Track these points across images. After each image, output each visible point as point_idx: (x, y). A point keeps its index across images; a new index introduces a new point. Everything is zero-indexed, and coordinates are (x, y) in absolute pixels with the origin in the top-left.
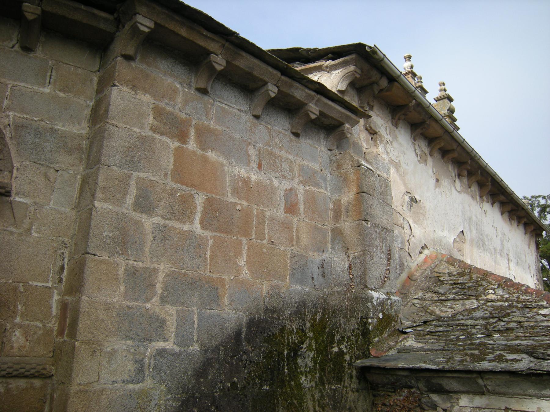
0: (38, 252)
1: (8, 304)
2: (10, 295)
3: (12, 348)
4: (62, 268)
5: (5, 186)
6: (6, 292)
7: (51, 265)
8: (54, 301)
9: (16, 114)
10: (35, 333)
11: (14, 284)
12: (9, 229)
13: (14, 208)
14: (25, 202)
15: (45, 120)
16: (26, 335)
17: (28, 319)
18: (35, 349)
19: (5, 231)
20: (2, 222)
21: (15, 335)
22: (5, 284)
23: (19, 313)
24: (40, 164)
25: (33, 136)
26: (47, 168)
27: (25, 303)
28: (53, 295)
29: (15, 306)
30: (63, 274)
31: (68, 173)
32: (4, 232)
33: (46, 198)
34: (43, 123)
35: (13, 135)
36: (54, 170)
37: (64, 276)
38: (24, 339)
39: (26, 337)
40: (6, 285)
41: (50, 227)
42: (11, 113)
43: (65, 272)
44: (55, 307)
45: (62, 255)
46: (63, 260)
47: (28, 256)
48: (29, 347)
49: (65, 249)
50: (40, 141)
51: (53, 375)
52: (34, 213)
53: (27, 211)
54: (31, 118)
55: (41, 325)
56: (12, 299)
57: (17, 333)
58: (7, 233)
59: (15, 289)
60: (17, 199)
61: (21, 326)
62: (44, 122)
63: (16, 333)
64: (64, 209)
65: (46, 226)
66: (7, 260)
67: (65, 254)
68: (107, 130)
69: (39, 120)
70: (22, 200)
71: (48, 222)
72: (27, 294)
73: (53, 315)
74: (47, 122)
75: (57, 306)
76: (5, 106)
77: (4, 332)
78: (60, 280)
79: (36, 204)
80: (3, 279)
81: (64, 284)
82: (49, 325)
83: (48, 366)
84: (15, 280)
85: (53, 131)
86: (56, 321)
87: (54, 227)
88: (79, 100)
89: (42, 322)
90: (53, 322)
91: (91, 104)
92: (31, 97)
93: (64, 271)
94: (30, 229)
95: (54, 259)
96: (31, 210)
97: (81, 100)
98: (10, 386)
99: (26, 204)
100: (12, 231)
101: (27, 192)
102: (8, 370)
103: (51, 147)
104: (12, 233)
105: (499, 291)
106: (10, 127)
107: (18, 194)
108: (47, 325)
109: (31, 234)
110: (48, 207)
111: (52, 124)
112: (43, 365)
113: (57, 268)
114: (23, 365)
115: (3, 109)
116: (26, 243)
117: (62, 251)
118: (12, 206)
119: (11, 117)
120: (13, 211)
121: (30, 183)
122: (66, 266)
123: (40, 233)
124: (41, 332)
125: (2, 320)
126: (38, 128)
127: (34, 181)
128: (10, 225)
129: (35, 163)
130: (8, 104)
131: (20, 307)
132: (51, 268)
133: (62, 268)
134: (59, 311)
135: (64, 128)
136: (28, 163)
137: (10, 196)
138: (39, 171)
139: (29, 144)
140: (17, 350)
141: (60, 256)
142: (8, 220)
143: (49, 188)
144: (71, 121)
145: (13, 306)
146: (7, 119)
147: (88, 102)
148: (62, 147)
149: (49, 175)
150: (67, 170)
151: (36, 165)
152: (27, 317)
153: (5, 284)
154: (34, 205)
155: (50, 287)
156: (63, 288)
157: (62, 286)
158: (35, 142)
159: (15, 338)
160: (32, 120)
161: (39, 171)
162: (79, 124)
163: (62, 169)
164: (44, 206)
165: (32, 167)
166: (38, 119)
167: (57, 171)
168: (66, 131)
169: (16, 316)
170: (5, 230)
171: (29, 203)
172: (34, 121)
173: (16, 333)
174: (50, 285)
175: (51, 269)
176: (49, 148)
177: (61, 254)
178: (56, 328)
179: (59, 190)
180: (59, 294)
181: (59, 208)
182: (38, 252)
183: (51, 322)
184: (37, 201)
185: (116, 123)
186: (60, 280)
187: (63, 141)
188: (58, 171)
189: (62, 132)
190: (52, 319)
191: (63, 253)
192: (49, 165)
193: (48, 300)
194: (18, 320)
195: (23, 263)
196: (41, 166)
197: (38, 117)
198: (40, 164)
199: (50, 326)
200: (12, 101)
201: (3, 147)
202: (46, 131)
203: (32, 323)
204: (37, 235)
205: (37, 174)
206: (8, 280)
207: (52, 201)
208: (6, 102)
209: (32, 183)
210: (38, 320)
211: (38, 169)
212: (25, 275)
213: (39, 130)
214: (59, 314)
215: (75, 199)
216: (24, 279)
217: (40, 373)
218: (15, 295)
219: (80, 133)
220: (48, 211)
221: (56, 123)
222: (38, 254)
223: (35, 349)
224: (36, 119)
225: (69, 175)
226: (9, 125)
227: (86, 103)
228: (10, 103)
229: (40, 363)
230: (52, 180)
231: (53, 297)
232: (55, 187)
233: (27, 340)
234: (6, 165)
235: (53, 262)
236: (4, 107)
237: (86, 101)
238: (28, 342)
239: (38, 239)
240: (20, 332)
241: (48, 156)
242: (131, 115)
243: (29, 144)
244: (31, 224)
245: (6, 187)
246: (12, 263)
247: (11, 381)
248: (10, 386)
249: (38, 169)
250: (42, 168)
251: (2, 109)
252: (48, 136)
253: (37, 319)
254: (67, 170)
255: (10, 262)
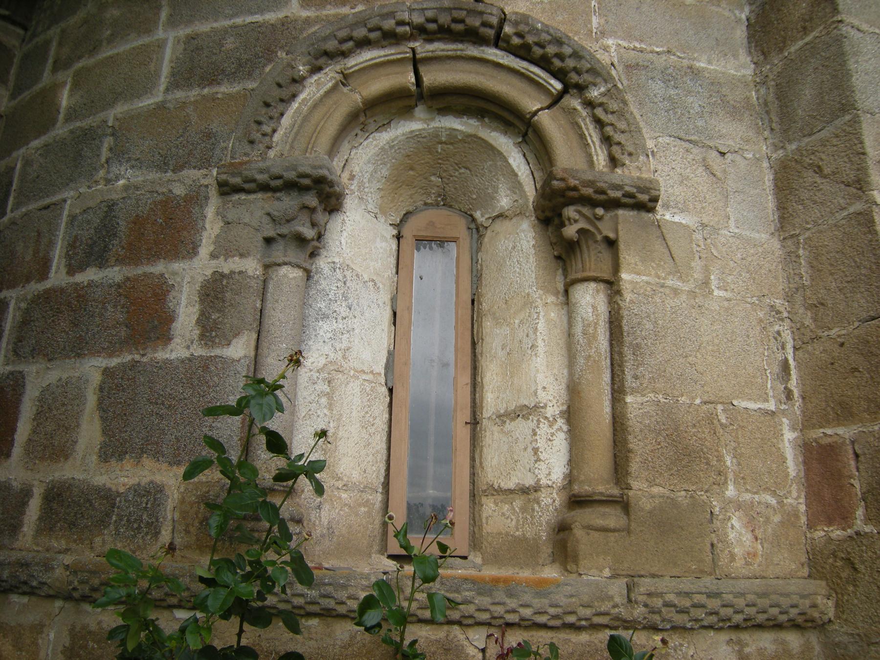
0: (733, 332)
1: (704, 454)
2: (704, 432)
3: (732, 557)
4: (785, 366)
5: (648, 185)
6: (694, 426)
7: (763, 360)
8: (787, 444)
9: (620, 42)
10: (767, 520)
11: (704, 407)
12: (669, 283)
13: (667, 236)
14: (684, 222)
15: (674, 50)
16: (751, 524)
17: (749, 488)
18: (776, 560)
19: (662, 287)
20: (652, 267)
21: (733, 527)
22: (689, 407)
23: (731, 476)
24: (690, 141)
25: (662, 84)
26: (704, 149)
27: (735, 449)
28: (781, 430)
29: (720, 458)
30: (789, 380)
31: (745, 158)
32: (662, 290)
33: (719, 212)
34: (672, 57)
35: (625, 85)
36: (717, 153)
37: (793, 383)
38: (749, 536)
39: (752, 531)
40: (691, 410)
41: (741, 275)
42: (610, 42)
43: (793, 372)
44: (792, 457)
45: (779, 338)
46: (783, 348)
47: (716, 341)
48: (762, 555)
49: (781, 323)
50: (678, 95)
51: (830, 621)
52: (705, 245)
53: (691, 242)
54: (649, 49)
55: (773, 501)
56: (709, 442)
57: (735, 521)
58: (667, 291)
59: (711, 418)
60: (668, 217)
61: (739, 506)
62: (674, 55)
63: (733, 522)
64: (757, 236)
65: (734, 273)
66: (681, 352)
67: (782, 334)
68: (846, 37)
69: (664, 52)
70: (677, 219)
71: (736, 265)
72: (733, 429)
73: (791, 477)
74: (678, 54)
75: (795, 455)
76: (597, 28)
77: (711, 521)
78: (789, 394)
79: (704, 225)
80: (682, 396)
81: (797, 404)
82: (789, 500)
83: (819, 598)
84: (706, 398)
85: (695, 73)
86: (798, 490)
87: (748, 275)
88: (721, 10)
89: (774, 494)
90: (795, 494)
91: (743, 17)
92: (637, 9)
93: (790, 375)
94: (706, 283)
95: (766, 347)
96: (698, 240)
97: (724, 9)
98: (747, 650)
99: (686, 227)
100: (675, 287)
101: (682, 202)
102: (747, 610)
103: (700, 106)
104: (676, 292)
105: (475, 556)
106: (615, 68)
107: (666, 206)
108: (785, 501)
109: (711, 292)
110: (727, 233)
111: (689, 59)
112: (811, 597)
113: (776, 369)
114: (773, 597)
115: (594, 34)
116: (706, 312)
117: (777, 328)
118: (662, 232)
119: (613, 50)
120: (667, 244)
121: (682, 182)
122: (791, 362)
123: (726, 290)
124: (777, 519)
125: (703, 493)
126: (666, 68)
127: (688, 177)
128: (670, 273)
129: (680, 139)
130: (599, 23)
131: (728, 461)
132: (766, 367)
133: (785, 366)
134: (802, 467)
135: (712, 65)
136: (667, 140)
137: (652, 210)
138: (691, 156)
139: (660, 102)
140: (743, 562)
141: (776, 339)
142: (662, 263)
143: (718, 190)
144: (721, 52)
145: (715, 458)
146: (606, 54)
147: (737, 12)
148: (719, 104)
149: (711, 163)
150: (741, 152)
151: (683, 143)
152: (744, 483)
153: (689, 407)
154: (701, 228)
155: (772, 412)
156: (798, 413)
157: (796, 408)
158: (670, 96)
159: (734, 535)
160: (652, 52)
161: (691, 156)
162: (735, 56)
163: (732, 150)
164: (719, 229)
165: (676, 149)
166: (661, 49)
167: (723, 154)
168: (716, 71)
169: (726, 482)
170: (662, 286)
171: (691, 224)
172: (655, 55)
173: (733, 522)
174: (771, 406)
175: (766, 370)
176: (697, 109)
177: (776, 335)
178: (803, 508)
179: (737, 194)
180: (793, 428)
181: (748, 233)
182: (733, 332)
183: (790, 492)
184: (705, 221)
185: (856, 22)
186: (789, 394)
187: (718, 92)
188: (724, 154)
189: (710, 73)
190: (791, 486)
191: (778, 333)
192: (708, 143)
193: (775, 441)
194: (731, 491)
195: (710, 358)
196: (692, 145)
197: (662, 47)
198: (690, 141)
199: (791, 504)
200: (605, 18)
201: (621, 105)
202: (683, 73)
203: (756, 497)
204: (722, 293)
205: (689, 162)
206: (693, 399)
207: (732, 219)
208: (595, 21)
209: (685, 182)
210: (767, 489)
211: (687, 151)
212: (721, 386)
213: (670, 71)
214: (802, 474)
215: (770, 212)
216: (721, 394)
217: (808, 617)
218: (712, 432)
219: (742, 74)
220: (728, 240)
221: (696, 55)
222: (734, 337)
223: (776, 560)
224: (658, 50)
225: (747, 162)
226: (612, 64)
227: (735, 15)
228: (602, 21)
229: (806, 593)
230: (718, 174)
231: (782, 435)
232: (729, 189)
233: (756, 539)
234: (637, 142)
235: (766, 354)
236: (595, 30)
237: (733, 12)
238: (759, 541)
239: (726, 304)
240: (739, 518)
241: (700, 123)
242: (873, 6)
243: (660, 102)
244: (707, 270)
245: (651, 189)
246: (691, 358)
247: (745, 636)
248: (747, 650)
249: (687, 151)
250: (695, 150)
251: (592, 35)
252: (688, 82)
253: (764, 487)
254: (741, 152)
255: (686, 357)
